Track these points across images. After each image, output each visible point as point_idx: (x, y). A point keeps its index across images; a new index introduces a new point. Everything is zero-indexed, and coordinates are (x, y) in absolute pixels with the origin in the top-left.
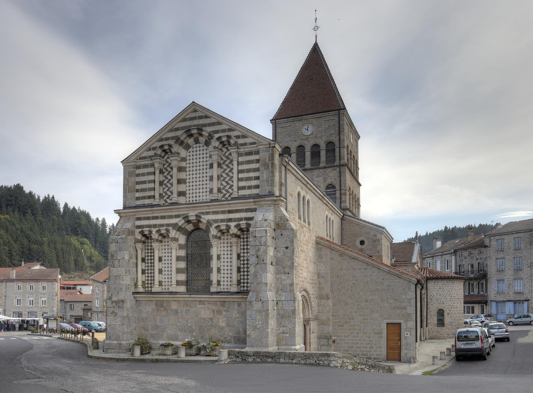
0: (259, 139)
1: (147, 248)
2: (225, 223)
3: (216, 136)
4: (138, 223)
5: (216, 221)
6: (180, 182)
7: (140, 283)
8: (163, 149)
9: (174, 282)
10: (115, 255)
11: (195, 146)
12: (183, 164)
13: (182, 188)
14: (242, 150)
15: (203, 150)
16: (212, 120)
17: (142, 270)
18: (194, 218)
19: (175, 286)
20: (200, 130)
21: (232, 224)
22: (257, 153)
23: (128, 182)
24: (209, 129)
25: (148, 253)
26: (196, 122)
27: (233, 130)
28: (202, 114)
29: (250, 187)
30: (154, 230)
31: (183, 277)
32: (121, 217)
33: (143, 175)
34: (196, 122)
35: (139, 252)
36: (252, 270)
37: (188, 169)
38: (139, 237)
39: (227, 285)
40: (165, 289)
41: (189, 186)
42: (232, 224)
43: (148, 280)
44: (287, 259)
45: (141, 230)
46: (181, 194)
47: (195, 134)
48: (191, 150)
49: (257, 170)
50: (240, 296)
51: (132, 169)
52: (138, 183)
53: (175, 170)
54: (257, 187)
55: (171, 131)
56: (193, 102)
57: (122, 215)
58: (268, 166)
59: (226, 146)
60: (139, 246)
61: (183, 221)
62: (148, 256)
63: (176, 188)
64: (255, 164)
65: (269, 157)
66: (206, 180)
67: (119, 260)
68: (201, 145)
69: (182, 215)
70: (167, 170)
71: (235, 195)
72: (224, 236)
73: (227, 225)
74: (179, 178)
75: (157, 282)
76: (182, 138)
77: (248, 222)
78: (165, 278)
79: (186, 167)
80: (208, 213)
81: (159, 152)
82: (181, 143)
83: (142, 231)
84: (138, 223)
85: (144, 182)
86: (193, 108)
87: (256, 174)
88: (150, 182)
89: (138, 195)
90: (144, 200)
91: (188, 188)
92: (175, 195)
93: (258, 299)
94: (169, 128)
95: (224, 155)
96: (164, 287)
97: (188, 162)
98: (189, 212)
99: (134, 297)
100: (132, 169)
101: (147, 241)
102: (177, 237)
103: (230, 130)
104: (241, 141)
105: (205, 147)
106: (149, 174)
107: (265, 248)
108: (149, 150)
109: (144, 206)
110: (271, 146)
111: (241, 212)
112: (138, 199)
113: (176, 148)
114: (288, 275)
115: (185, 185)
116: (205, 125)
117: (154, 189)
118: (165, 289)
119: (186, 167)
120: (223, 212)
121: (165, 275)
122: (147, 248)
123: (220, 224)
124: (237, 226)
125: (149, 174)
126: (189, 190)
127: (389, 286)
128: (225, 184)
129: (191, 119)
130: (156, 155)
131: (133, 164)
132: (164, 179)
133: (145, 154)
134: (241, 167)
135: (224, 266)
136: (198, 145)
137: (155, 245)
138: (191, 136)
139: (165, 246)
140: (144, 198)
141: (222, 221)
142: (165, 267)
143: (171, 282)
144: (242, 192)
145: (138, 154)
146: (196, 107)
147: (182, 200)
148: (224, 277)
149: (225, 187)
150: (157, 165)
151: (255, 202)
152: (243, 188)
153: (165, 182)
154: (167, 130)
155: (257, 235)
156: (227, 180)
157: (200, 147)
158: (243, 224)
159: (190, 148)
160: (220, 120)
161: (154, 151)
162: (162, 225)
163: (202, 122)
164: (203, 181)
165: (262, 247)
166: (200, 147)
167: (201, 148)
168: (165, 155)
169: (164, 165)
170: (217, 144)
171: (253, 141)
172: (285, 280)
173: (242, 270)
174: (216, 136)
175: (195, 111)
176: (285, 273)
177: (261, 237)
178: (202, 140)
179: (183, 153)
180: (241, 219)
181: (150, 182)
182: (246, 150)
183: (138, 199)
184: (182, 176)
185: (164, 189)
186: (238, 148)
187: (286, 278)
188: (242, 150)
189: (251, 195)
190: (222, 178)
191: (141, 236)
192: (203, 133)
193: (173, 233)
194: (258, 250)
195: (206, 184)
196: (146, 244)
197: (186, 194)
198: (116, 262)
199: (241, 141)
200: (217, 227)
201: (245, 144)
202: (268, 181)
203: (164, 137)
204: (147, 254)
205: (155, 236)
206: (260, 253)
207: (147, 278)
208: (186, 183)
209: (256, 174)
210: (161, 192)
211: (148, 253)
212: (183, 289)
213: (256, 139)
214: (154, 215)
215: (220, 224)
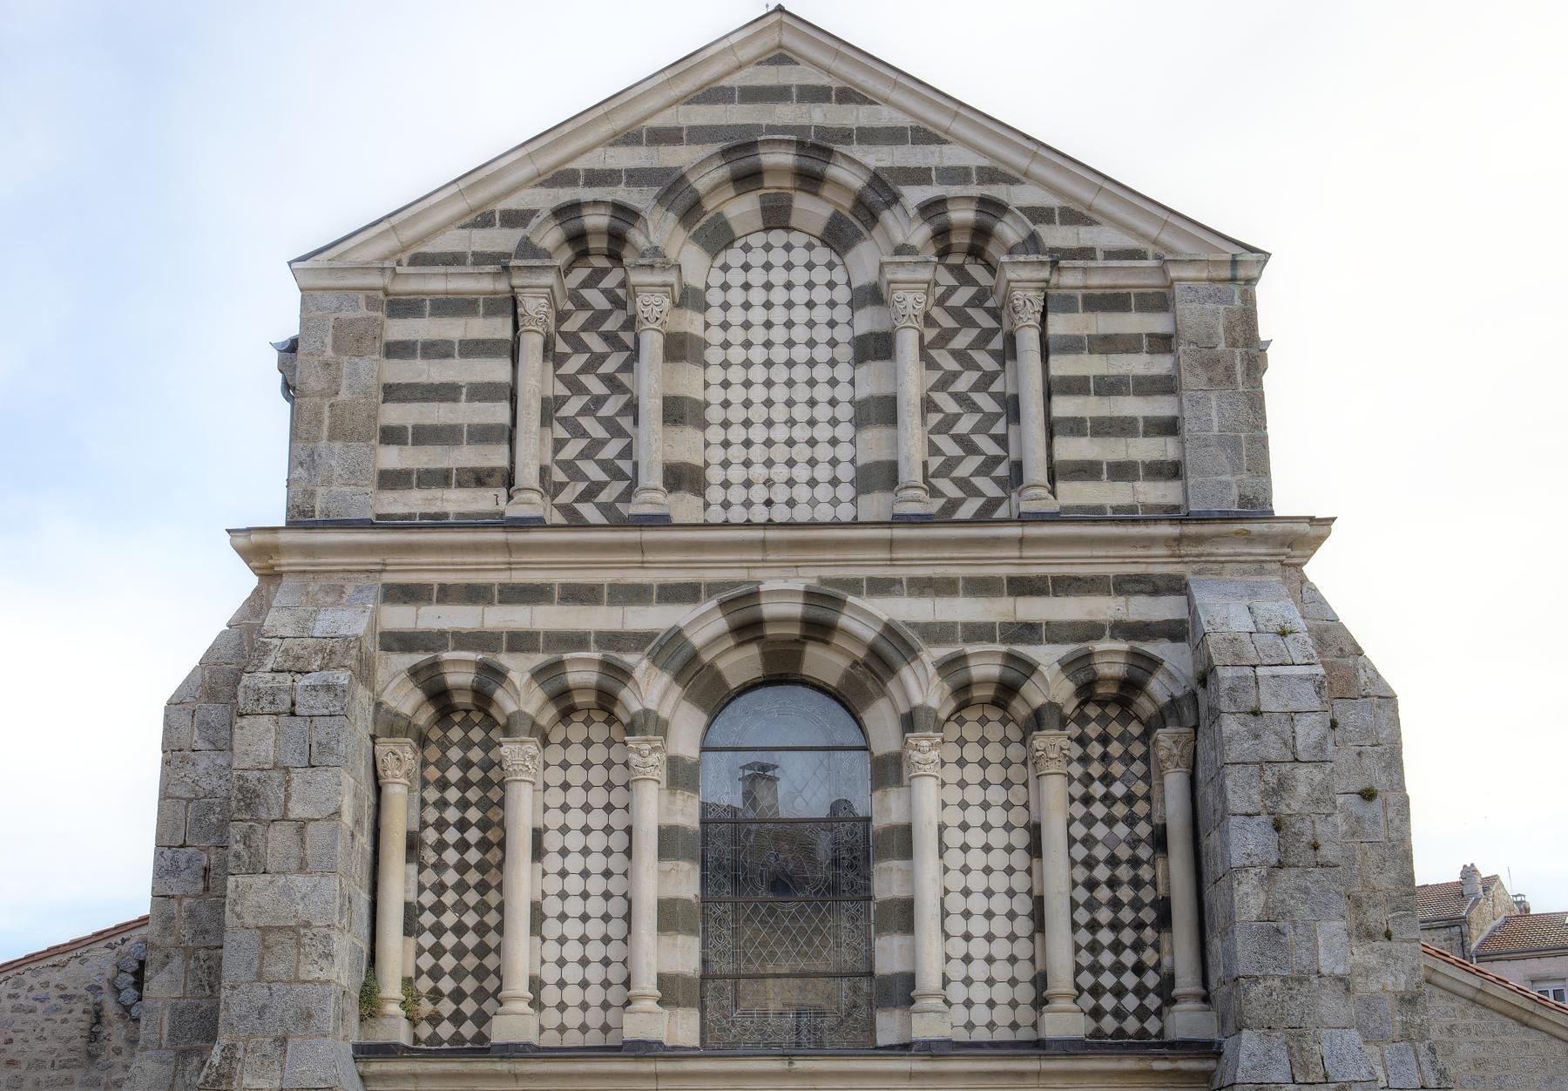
0: (1166, 237)
1: (433, 773)
2: (1004, 648)
3: (914, 195)
4: (401, 618)
5: (937, 633)
6: (677, 412)
7: (391, 989)
8: (573, 225)
9: (646, 983)
10: (274, 793)
11: (757, 240)
12: (692, 323)
13: (687, 446)
14: (1070, 279)
15: (810, 266)
16: (885, 117)
17: (407, 905)
18: (796, 609)
19: (650, 1004)
20: (816, 150)
21: (1047, 656)
22: (1160, 301)
23: (335, 380)
24: (879, 157)
25: (442, 804)
26: (786, 114)
27: (1011, 181)
28: (824, 80)
29: (1122, 471)
30: (518, 667)
31: (684, 955)
32: (270, 576)
33: (437, 350)
34: (786, 114)
35: (398, 793)
36: (1248, 899)
37: (714, 355)
38: (407, 700)
39: (991, 1004)
40: (562, 1029)
41: (726, 444)
42: (1047, 656)
43: (436, 973)
44: (1374, 856)
45: (419, 658)
46: (681, 478)
47: (778, 170)
48: (734, 256)
49: (1167, 386)
50: (1129, 1064)
51: (363, 312)
52: (392, 393)
53: (652, 344)
54: (1172, 471)
55: (629, 138)
56: (780, 9)
57: (286, 562)
58: (1229, 371)
59: (954, 260)
60: (400, 759)
61: (720, 624)
62: (441, 825)
63: (657, 445)
64: (1144, 357)
65: (1230, 329)
66: (834, 422)
67: (302, 825)
68: (798, 239)
69: (713, 588)
70: (579, 346)
71: (1035, 498)
72: (961, 722)
73: (1011, 658)
74: (671, 393)
75: (518, 985)
76: (701, 183)
77: (1138, 645)
78: (561, 962)
79: (706, 345)
80: (881, 587)
81: (550, 237)
82: (691, 211)
83: (435, 665)
84: (401, 618)
85: (447, 393)
86: (770, 40)
87: (1162, 407)
88: (483, 392)
89: (391, 458)
90: (435, 492)
91: (717, 454)
92: (652, 477)
93: (1305, 1068)
94: (620, 122)
95: (940, 302)
96: (552, 1018)
97: (715, 315)
98: (758, 574)
99: (362, 1077)
100: (363, 312)
101: (435, 734)
102: (665, 713)
103: (990, 175)
104: (1057, 236)
105: (822, 255)
106: (473, 348)
107: (1318, 776)
108: (484, 220)
109: (438, 522)
110: (1241, 273)
111: (1089, 592)
112: (392, 480)
113: (660, 229)
114: (1386, 945)
115: (700, 434)
116: (845, 135)
117: (509, 435)
118: (562, 1029)
119: (706, 345)
120: (981, 587)
121: (562, 940)
122: (433, 773)
123: (970, 649)
124: (1078, 666)
125: (473, 348)
126: (726, 464)
127: (1478, 1064)
128: (951, 448)
129: (753, 95)
130: (527, 248)
131: (376, 280)
132: (562, 390)
133: (450, 242)
134: (1062, 366)
135: (966, 892)
136: (778, 237)
137: (517, 753)
138: (747, 179)
139: (565, 765)
140: (441, 478)
141: (978, 632)
142: (563, 895)
143: (627, 984)
144: (1074, 493)
145: (408, 234)
146: (789, 40)
147: (684, 507)
148: (967, 959)
149: (951, 464)
150: (533, 305)
151: (1179, 540)
152: (1086, 471)
153: (571, 408)
154: (605, 130)
155: (1268, 703)
156: (965, 425)
157: (788, 247)
158: (1111, 657)
159: (729, 244)
160: (934, 117)
161: (517, 234)
162: (578, 640)
163: (819, 115)
164: (812, 423)
165: (1302, 772)
166: (788, 247)
167: (800, 256)
168: (569, 269)
169: (562, 317)
170: (920, 234)
171: (1130, 242)
172: (1368, 972)
173: (1148, 915)
174: (914, 195)
175: (781, 58)
176: (1370, 935)
177: (1292, 715)
178: (811, 211)
179: (695, 265)
180: (1093, 631)
181: (483, 392)
182: (1095, 280)
183: (392, 480)
184: (688, 381)
185: (559, 444)
186: (1054, 265)
187: (1373, 960)
188: (1070, 279)
189: (1132, 509)
190: (934, 418)
191: (418, 696)
192: (838, 171)
193: (651, 689)
194: (1282, 787)
195: (834, 442)
196: (433, 753)
197: (706, 484)
198: (278, 840)
199: (1057, 236)
200: (950, 666)
201: (1086, 253)
202: (1235, 444)
203: (580, 164)
204: (432, 815)
205: (521, 695)
206: (1293, 805)
207: (427, 961)
208: (704, 425)
209: (1162, 407)
210: (548, 461)
211: (442, 804)
212: (683, 1027)
213: (1143, 236)
214: (519, 577)
215: (970, 649)
